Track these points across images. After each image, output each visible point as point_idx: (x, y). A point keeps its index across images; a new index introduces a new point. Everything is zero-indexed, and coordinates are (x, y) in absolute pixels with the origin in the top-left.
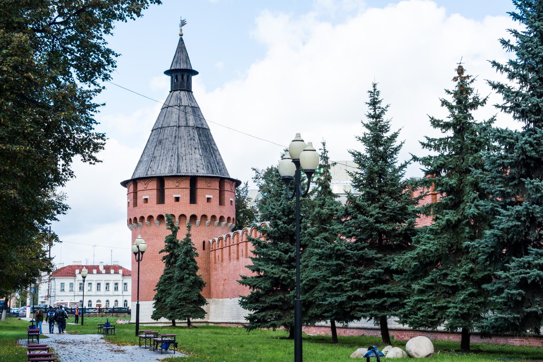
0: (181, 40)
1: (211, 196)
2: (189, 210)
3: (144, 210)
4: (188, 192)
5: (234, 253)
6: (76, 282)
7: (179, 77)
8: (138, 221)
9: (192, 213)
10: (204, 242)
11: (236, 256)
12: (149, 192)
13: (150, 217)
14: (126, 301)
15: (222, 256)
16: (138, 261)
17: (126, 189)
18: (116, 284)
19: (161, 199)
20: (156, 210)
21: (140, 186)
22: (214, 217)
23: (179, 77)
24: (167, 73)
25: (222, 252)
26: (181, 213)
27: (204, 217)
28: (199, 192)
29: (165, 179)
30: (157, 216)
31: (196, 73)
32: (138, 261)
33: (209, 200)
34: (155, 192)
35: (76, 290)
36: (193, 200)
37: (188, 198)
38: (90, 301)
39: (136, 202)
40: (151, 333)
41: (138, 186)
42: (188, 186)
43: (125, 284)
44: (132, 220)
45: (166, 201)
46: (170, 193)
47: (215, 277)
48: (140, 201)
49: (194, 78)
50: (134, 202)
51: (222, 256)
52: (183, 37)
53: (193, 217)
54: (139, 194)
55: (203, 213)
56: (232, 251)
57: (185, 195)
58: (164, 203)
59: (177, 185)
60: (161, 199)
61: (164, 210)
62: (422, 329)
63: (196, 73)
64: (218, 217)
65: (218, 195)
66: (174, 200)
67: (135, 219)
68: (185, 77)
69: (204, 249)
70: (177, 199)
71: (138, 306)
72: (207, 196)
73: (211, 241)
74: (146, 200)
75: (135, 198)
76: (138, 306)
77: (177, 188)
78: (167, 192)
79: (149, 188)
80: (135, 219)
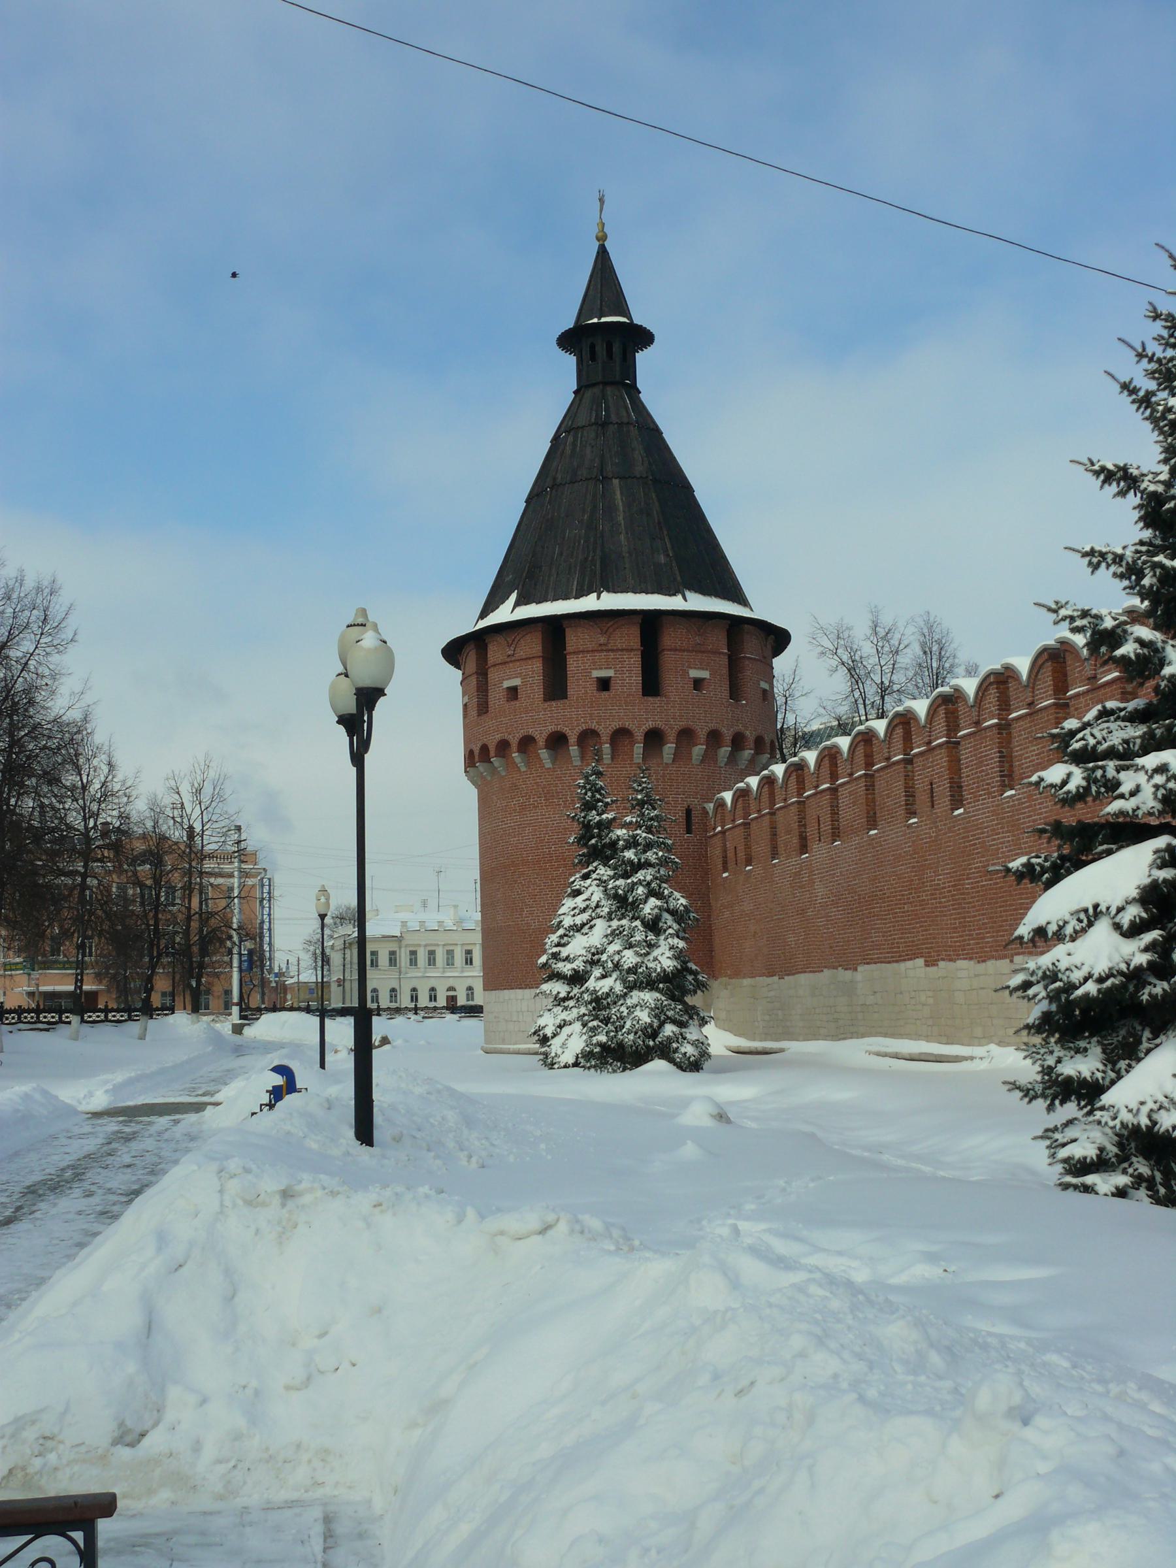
0: (603, 258)
2: (642, 716)
3: (508, 724)
5: (788, 832)
6: (403, 950)
7: (601, 350)
8: (492, 753)
9: (650, 724)
10: (688, 812)
11: (795, 840)
12: (521, 673)
13: (527, 743)
15: (748, 847)
17: (460, 672)
19: (556, 688)
20: (543, 719)
21: (495, 652)
22: (714, 737)
23: (601, 350)
25: (747, 836)
26: (616, 725)
27: (686, 735)
28: (669, 661)
29: (565, 623)
30: (545, 735)
33: (698, 684)
34: (538, 666)
35: (403, 964)
36: (651, 685)
37: (635, 678)
38: (433, 989)
39: (487, 703)
41: (490, 654)
44: (477, 752)
45: (570, 692)
46: (583, 669)
47: (727, 914)
48: (496, 697)
49: (643, 359)
50: (479, 703)
51: (748, 847)
52: (606, 244)
53: (654, 738)
54: (493, 675)
55: (683, 724)
56: (781, 829)
57: (626, 671)
59: (603, 640)
60: (556, 688)
61: (569, 717)
62: (266, 947)
64: (728, 734)
65: (725, 671)
66: (592, 688)
67: (484, 749)
68: (617, 349)
69: (689, 831)
70: (604, 684)
72: (694, 673)
73: (710, 807)
74: (513, 692)
75: (824, 1250)
77: (602, 648)
78: (573, 664)
79: (521, 653)
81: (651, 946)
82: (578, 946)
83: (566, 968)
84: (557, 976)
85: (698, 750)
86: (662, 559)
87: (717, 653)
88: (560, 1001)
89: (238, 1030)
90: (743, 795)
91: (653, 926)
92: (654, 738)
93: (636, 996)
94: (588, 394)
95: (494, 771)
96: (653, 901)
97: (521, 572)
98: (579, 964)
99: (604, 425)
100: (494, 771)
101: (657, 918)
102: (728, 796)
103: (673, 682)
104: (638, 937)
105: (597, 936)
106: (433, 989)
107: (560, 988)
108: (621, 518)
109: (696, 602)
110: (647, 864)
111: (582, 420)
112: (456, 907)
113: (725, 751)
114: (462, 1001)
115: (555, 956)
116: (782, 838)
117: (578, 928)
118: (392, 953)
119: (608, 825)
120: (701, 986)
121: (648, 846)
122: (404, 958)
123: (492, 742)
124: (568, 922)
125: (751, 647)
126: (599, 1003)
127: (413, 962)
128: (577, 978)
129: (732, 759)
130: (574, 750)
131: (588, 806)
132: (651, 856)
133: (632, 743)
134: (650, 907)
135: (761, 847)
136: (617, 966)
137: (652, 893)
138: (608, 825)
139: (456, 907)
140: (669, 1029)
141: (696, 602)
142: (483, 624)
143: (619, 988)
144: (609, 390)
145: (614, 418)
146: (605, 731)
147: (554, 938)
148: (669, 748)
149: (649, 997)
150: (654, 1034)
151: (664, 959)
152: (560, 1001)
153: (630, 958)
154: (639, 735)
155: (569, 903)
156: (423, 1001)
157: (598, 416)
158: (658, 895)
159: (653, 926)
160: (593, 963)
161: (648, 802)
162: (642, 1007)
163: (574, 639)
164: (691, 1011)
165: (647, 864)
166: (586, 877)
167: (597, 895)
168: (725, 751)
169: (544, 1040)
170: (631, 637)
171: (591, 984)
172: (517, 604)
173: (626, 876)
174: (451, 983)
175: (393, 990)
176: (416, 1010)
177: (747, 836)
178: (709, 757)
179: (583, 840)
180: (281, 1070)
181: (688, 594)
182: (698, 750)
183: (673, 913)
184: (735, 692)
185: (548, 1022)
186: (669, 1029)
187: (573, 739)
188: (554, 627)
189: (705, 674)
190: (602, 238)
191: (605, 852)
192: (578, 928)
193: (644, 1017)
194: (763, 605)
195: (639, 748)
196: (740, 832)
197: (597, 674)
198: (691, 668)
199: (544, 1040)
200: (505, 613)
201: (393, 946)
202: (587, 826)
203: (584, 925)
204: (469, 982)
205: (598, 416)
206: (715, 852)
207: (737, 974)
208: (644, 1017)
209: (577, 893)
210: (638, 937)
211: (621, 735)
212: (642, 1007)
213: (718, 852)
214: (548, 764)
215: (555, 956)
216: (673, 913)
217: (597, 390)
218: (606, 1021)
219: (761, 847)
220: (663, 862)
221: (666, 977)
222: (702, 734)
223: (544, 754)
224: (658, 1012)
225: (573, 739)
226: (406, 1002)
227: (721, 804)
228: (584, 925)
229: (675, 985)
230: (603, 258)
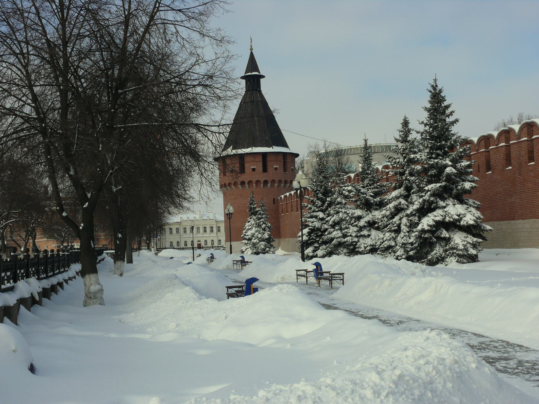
0: (252, 55)
1: (255, 167)
2: (262, 177)
4: (261, 164)
10: (274, 199)
14: (220, 240)
16: (230, 219)
18: (212, 227)
22: (280, 182)
24: (242, 78)
25: (287, 206)
26: (256, 179)
27: (273, 181)
28: (269, 164)
31: (263, 77)
32: (230, 219)
33: (276, 169)
36: (265, 170)
40: (534, 380)
42: (261, 159)
43: (219, 227)
46: (249, 166)
53: (266, 182)
55: (272, 179)
57: (259, 167)
58: (244, 173)
63: (263, 77)
64: (283, 180)
65: (282, 165)
66: (251, 171)
67: (225, 184)
68: (256, 80)
70: (254, 170)
71: (231, 246)
72: (275, 166)
76: (231, 246)
78: (246, 165)
80: (225, 184)
81: (264, 233)
82: (249, 233)
83: (247, 237)
84: (245, 239)
85: (276, 185)
86: (267, 138)
87: (280, 161)
88: (246, 244)
89: (156, 254)
90: (286, 196)
91: (264, 229)
92: (266, 182)
93: (261, 243)
94: (249, 93)
95: (227, 189)
96: (264, 225)
97: (233, 140)
98: (250, 237)
99: (253, 102)
100: (227, 189)
101: (265, 228)
102: (283, 196)
103: (270, 169)
104: (261, 232)
105: (254, 230)
106: (186, 242)
107: (246, 241)
108: (257, 127)
109: (276, 149)
110: (263, 218)
111: (247, 100)
112: (200, 211)
113: (283, 184)
114: (203, 244)
115: (245, 235)
116: (293, 208)
117: (249, 229)
118: (177, 229)
119: (255, 208)
120: (273, 241)
121: (263, 214)
122: (182, 231)
123: (227, 183)
124: (247, 228)
125: (289, 160)
126: (254, 245)
127: (185, 232)
128: (250, 239)
129: (284, 186)
130: (247, 185)
131: (251, 204)
132: (263, 216)
133: (261, 183)
134: (264, 226)
135: (289, 209)
136: (257, 237)
137: (264, 223)
138: (255, 208)
139: (200, 211)
140: (267, 249)
141: (276, 149)
142: (224, 153)
143: (258, 241)
144: (254, 92)
145: (255, 100)
146: (254, 181)
147: (244, 231)
148: (269, 185)
149: (263, 243)
150: (265, 250)
151: (266, 236)
152: (246, 244)
153: (260, 236)
154: (262, 182)
155: (247, 224)
156: (216, 244)
157: (251, 99)
158: (265, 224)
159: (264, 229)
160: (252, 236)
161: (263, 206)
162: (262, 245)
163: (247, 159)
164: (272, 246)
165: (263, 218)
166: (251, 218)
167: (253, 222)
168: (283, 184)
169: (243, 252)
170: (260, 159)
171: (252, 241)
172: (233, 149)
173: (259, 220)
174: (199, 239)
175: (178, 242)
176: (213, 247)
177: (287, 206)
178: (279, 186)
179: (250, 211)
180: (212, 254)
181: (274, 147)
182: (276, 185)
183: (268, 227)
184: (285, 170)
185: (244, 248)
186: (267, 249)
187: (246, 183)
188: (242, 156)
189: (278, 166)
190: (251, 49)
191: (255, 213)
192: (249, 229)
193: (263, 247)
194: (292, 148)
195: (262, 185)
196: (285, 205)
197: (252, 167)
198: (274, 165)
199: (243, 252)
200: (230, 151)
201: (178, 226)
202: (251, 208)
203: (251, 228)
204: (212, 238)
205: (251, 99)
206: (280, 209)
207: (285, 237)
208: (263, 247)
209: (249, 222)
210: (261, 232)
211: (258, 182)
212: (262, 245)
213: (281, 209)
214: (241, 188)
215: (245, 235)
216: (268, 227)
217: (251, 92)
218: (255, 248)
219: (289, 209)
220: (266, 217)
221: (266, 239)
222: (277, 181)
223: (240, 186)
224: (265, 246)
225: (246, 183)
226: (182, 245)
227: (281, 198)
228: (251, 228)
229: (269, 241)
230: (252, 55)
